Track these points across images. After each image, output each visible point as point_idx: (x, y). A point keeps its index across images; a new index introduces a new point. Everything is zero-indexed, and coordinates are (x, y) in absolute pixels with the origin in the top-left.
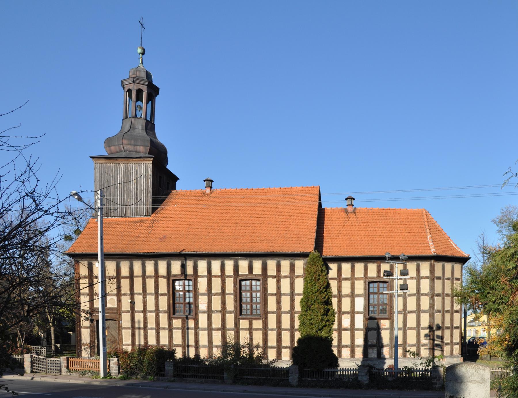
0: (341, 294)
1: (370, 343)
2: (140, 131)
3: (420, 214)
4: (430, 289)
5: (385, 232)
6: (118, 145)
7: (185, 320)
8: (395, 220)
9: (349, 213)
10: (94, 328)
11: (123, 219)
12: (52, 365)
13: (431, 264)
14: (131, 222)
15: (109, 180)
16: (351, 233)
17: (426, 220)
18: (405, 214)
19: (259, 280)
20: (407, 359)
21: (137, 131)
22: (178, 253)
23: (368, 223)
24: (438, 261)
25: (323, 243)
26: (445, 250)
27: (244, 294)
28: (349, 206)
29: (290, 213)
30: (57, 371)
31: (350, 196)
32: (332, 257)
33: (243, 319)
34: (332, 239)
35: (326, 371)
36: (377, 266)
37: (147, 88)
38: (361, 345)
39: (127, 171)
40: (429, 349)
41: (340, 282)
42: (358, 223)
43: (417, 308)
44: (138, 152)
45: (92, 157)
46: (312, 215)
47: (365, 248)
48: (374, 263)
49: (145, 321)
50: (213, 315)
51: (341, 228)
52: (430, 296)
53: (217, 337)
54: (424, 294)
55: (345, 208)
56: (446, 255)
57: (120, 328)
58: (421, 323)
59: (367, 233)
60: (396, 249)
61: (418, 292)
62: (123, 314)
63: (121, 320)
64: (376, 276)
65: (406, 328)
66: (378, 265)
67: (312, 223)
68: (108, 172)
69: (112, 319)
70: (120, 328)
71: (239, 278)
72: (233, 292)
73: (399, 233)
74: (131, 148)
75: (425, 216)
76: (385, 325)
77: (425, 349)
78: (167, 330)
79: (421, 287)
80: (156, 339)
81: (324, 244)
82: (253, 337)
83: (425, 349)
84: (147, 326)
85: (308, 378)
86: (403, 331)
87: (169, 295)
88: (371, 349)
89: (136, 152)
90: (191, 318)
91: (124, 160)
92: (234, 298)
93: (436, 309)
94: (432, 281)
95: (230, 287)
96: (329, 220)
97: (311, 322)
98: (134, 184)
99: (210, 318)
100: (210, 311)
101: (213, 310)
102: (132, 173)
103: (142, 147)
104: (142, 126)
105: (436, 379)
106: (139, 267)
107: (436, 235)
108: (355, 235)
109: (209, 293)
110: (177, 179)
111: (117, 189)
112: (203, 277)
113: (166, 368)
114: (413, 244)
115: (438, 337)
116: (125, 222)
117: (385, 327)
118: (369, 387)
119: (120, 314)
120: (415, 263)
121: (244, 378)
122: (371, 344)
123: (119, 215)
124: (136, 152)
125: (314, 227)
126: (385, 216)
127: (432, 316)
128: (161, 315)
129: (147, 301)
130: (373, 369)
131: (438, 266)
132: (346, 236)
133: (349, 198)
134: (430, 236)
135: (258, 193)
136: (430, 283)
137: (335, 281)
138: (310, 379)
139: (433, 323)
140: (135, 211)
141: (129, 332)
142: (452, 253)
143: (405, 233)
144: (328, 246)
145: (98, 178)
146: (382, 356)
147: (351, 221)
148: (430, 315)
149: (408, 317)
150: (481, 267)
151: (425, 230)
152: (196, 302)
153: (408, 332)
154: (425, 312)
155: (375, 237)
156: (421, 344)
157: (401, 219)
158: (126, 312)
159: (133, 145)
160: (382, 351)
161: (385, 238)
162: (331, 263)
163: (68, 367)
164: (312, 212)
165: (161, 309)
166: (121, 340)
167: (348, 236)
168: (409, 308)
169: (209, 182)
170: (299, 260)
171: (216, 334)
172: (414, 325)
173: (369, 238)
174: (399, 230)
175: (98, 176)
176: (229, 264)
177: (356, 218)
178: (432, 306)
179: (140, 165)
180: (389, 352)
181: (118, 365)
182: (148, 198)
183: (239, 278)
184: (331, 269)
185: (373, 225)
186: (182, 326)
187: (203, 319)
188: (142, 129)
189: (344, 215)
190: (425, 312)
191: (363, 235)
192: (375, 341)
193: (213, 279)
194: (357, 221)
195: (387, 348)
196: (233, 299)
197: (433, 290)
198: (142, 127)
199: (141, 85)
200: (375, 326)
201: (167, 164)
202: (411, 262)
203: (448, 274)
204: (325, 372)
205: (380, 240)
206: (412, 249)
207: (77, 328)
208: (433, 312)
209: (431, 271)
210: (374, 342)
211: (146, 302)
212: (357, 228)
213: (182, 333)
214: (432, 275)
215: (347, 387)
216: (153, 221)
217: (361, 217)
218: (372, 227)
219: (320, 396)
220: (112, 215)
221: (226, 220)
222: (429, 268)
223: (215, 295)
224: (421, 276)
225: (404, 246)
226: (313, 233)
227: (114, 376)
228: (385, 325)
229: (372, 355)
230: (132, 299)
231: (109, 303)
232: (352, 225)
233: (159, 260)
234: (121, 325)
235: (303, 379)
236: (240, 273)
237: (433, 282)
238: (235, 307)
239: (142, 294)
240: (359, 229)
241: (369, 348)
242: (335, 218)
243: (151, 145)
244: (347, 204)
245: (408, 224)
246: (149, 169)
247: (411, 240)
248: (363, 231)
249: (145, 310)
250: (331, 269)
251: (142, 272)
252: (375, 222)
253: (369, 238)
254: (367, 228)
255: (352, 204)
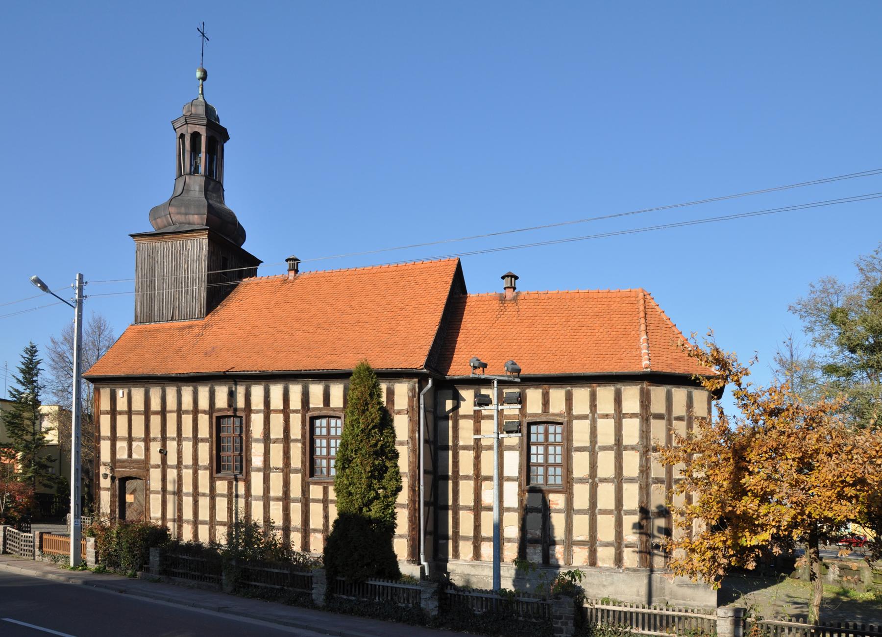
0: (479, 443)
1: (529, 536)
2: (197, 192)
3: (634, 299)
4: (641, 437)
5: (563, 332)
6: (165, 215)
7: (232, 483)
8: (584, 312)
9: (507, 302)
10: (116, 491)
11: (170, 324)
12: (25, 543)
13: (642, 390)
14: (178, 329)
15: (153, 268)
16: (503, 336)
17: (642, 308)
18: (605, 300)
19: (339, 418)
20: (597, 570)
21: (192, 193)
22: (223, 374)
23: (537, 318)
24: (656, 383)
25: (453, 355)
26: (673, 362)
27: (318, 441)
28: (507, 290)
29: (403, 305)
30: (28, 553)
31: (510, 272)
32: (462, 377)
33: (316, 483)
34: (469, 347)
35: (371, 585)
36: (543, 393)
37: (207, 129)
38: (514, 539)
39: (176, 251)
40: (640, 552)
41: (478, 422)
42: (519, 318)
43: (615, 474)
44: (192, 224)
45: (133, 236)
46: (436, 307)
47: (523, 361)
48: (537, 388)
49: (180, 483)
50: (272, 474)
51: (488, 328)
52: (641, 449)
53: (276, 512)
54: (630, 447)
55: (501, 294)
56: (673, 371)
57: (148, 492)
58: (624, 503)
59: (531, 335)
60: (577, 362)
61: (617, 443)
62: (152, 470)
63: (149, 480)
64: (540, 411)
65: (595, 511)
66: (545, 391)
67: (434, 319)
68: (152, 256)
69: (137, 476)
70: (147, 491)
71: (309, 415)
72: (300, 437)
73: (588, 334)
74: (181, 218)
75: (642, 302)
76: (557, 504)
77: (634, 552)
78: (208, 498)
79: (624, 432)
80: (193, 511)
81: (455, 356)
82: (330, 515)
83: (634, 552)
84: (182, 491)
85: (343, 594)
86: (590, 516)
87: (212, 442)
88: (532, 548)
89: (189, 224)
90: (241, 480)
91: (171, 236)
92: (302, 447)
93: (652, 476)
94: (645, 422)
95: (296, 431)
96: (471, 314)
97: (349, 489)
98: (185, 271)
99: (266, 480)
100: (267, 468)
101: (271, 466)
102: (183, 254)
103: (196, 216)
104: (200, 186)
105: (560, 621)
106: (173, 397)
107: (660, 335)
108: (509, 338)
109: (267, 439)
110: (258, 262)
111: (163, 279)
112: (258, 412)
113: (151, 558)
114: (611, 353)
115: (660, 530)
116: (170, 329)
117: (557, 507)
118: (438, 623)
119: (148, 470)
120: (613, 388)
121: (252, 585)
122: (531, 538)
123: (139, 320)
124: (189, 224)
125: (434, 326)
126: (570, 303)
127: (645, 491)
128: (200, 472)
129: (183, 450)
130: (449, 587)
131: (658, 393)
132: (493, 341)
133: (508, 276)
134: (645, 337)
135: (363, 276)
136: (642, 425)
137: (471, 420)
138: (345, 597)
139: (647, 503)
140: (184, 311)
141: (158, 499)
142: (687, 368)
143: (600, 334)
144: (461, 358)
145: (140, 266)
146: (552, 561)
147: (508, 316)
148: (641, 488)
149: (599, 489)
150: (39, 366)
151: (637, 327)
152: (249, 453)
153: (600, 518)
154: (631, 480)
155: (544, 341)
156: (625, 542)
157: (596, 309)
158: (156, 468)
159: (183, 214)
160: (551, 552)
161: (562, 343)
162: (463, 389)
163: (41, 548)
164: (438, 302)
165: (200, 463)
166: (148, 510)
167: (498, 341)
168: (601, 473)
169: (294, 264)
170: (401, 382)
171: (276, 507)
172: (611, 506)
173: (532, 344)
174: (589, 328)
175: (140, 262)
176: (296, 390)
177: (517, 310)
178: (645, 469)
179: (192, 241)
180: (565, 555)
181: (95, 549)
182: (200, 291)
183: (309, 415)
184: (464, 400)
185: (544, 321)
186: (228, 492)
187: (257, 479)
188: (200, 191)
189: (497, 305)
190: (631, 480)
191: (524, 338)
192: (538, 533)
193: (272, 416)
194: (517, 315)
195: (561, 546)
196: (300, 450)
197: (647, 439)
198: (200, 188)
199: (197, 126)
200: (539, 504)
201: (244, 240)
202: (605, 386)
203: (679, 409)
204: (370, 586)
205: (552, 346)
206: (608, 361)
207: (96, 489)
208: (647, 482)
209: (642, 402)
210: (536, 534)
211: (181, 451)
212: (516, 327)
213: (228, 503)
214: (645, 411)
215: (399, 620)
216: (206, 326)
217: (526, 307)
218: (542, 323)
219: (325, 632)
220: (156, 320)
221: (305, 320)
222: (639, 397)
223: (274, 443)
224: (624, 412)
225: (593, 356)
226: (430, 337)
227: (90, 565)
228: (557, 504)
229: (533, 559)
230: (164, 445)
231: (135, 452)
232: (507, 321)
233: (200, 386)
234: (148, 487)
235: (335, 595)
236: (311, 406)
237: (646, 423)
238: (303, 462)
239: (177, 439)
240: (518, 329)
241: (528, 544)
242: (481, 311)
243: (208, 212)
244: (505, 286)
245: (609, 316)
246: (204, 247)
247: (608, 345)
248: (524, 332)
249: (179, 466)
250: (464, 400)
251: (178, 405)
252: (549, 315)
253: (532, 344)
254: (534, 326)
255: (513, 285)
